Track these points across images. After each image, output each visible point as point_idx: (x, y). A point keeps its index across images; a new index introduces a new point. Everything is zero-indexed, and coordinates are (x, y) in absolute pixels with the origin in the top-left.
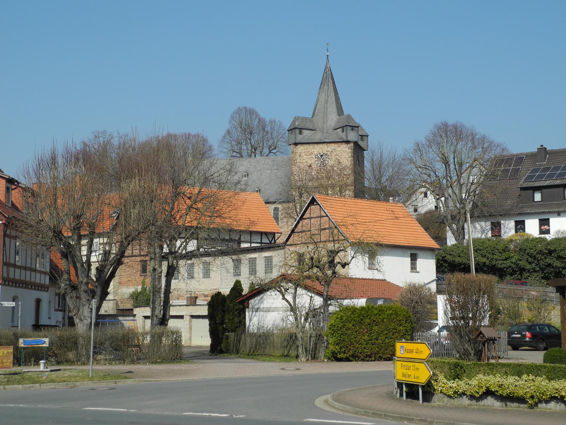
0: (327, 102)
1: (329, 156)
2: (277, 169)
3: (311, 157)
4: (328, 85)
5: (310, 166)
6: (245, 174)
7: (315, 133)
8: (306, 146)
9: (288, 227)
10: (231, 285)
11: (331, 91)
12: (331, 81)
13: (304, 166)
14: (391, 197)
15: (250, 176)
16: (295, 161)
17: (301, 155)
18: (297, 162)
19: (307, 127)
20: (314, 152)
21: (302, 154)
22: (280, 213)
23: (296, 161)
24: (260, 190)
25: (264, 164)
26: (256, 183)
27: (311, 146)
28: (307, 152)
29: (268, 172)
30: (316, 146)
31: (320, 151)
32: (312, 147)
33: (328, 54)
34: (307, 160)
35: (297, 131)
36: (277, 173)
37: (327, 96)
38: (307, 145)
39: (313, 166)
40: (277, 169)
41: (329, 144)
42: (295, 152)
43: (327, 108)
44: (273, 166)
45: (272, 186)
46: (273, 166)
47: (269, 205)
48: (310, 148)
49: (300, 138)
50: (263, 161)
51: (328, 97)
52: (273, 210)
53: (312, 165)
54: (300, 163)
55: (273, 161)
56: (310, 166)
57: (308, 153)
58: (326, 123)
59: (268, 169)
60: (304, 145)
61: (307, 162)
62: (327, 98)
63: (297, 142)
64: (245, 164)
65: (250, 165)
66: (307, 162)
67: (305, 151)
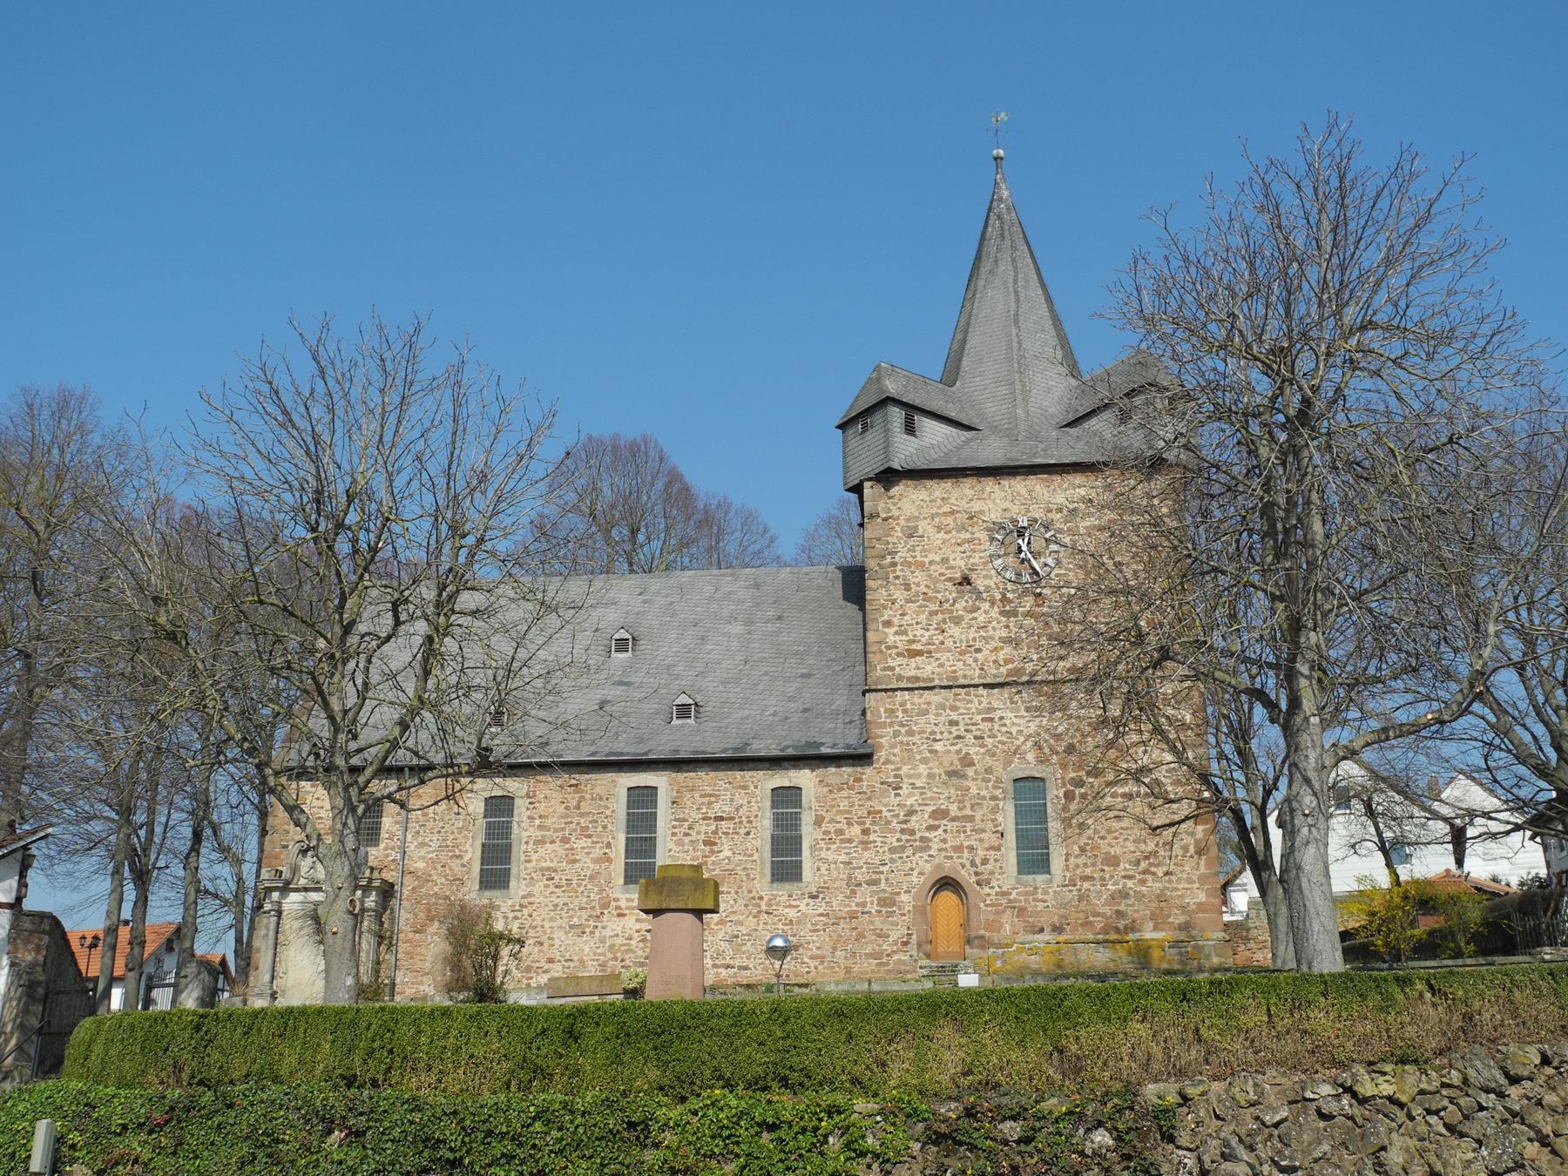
0: (1016, 322)
1: (1060, 531)
2: (780, 618)
3: (968, 536)
4: (1014, 260)
5: (966, 580)
6: (623, 634)
7: (969, 440)
8: (939, 489)
9: (853, 892)
10: (1465, 865)
11: (1027, 282)
12: (1023, 247)
13: (936, 581)
14: (968, 990)
15: (644, 645)
16: (883, 557)
17: (916, 528)
18: (894, 564)
19: (936, 405)
20: (982, 512)
21: (923, 526)
22: (807, 819)
23: (889, 559)
24: (696, 704)
25: (710, 599)
26: (678, 676)
27: (968, 487)
28: (945, 514)
29: (737, 629)
30: (989, 484)
31: (1015, 510)
32: (969, 492)
33: (1001, 152)
34: (946, 552)
35: (896, 415)
36: (778, 632)
37: (1012, 297)
38: (948, 484)
39: (980, 583)
40: (780, 618)
41: (1057, 479)
42: (883, 515)
43: (1019, 343)
44: (758, 605)
45: (761, 687)
46: (758, 605)
47: (748, 774)
48: (963, 493)
49: (905, 451)
50: (709, 589)
51: (1018, 301)
52: (768, 804)
53: (973, 577)
54: (909, 565)
55: (757, 586)
56: (966, 580)
57: (950, 520)
58: (1026, 401)
59: (732, 619)
60: (929, 483)
61: (945, 560)
62: (1013, 305)
63: (896, 466)
64: (624, 598)
65: (645, 602)
66: (945, 560)
67: (934, 511)
